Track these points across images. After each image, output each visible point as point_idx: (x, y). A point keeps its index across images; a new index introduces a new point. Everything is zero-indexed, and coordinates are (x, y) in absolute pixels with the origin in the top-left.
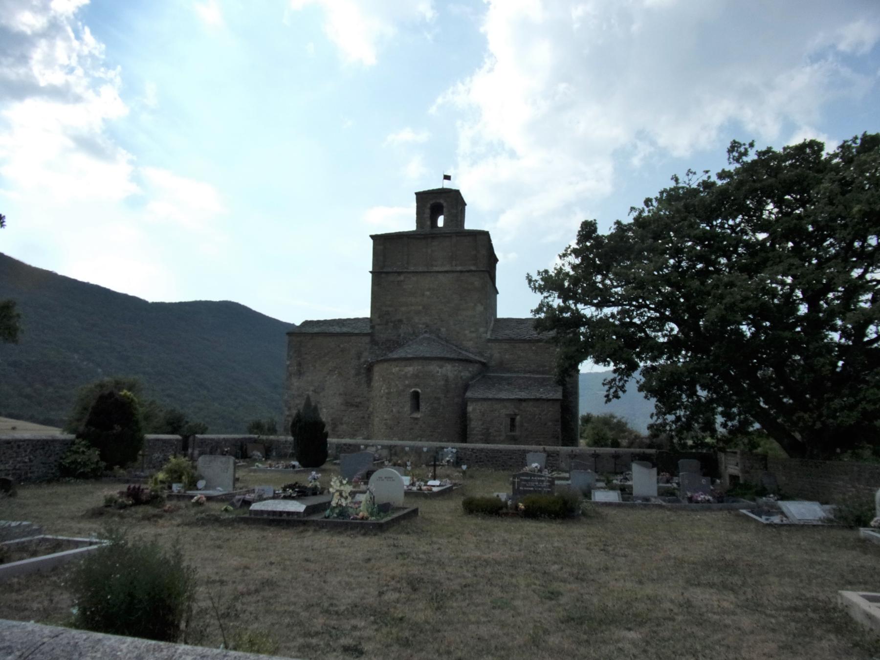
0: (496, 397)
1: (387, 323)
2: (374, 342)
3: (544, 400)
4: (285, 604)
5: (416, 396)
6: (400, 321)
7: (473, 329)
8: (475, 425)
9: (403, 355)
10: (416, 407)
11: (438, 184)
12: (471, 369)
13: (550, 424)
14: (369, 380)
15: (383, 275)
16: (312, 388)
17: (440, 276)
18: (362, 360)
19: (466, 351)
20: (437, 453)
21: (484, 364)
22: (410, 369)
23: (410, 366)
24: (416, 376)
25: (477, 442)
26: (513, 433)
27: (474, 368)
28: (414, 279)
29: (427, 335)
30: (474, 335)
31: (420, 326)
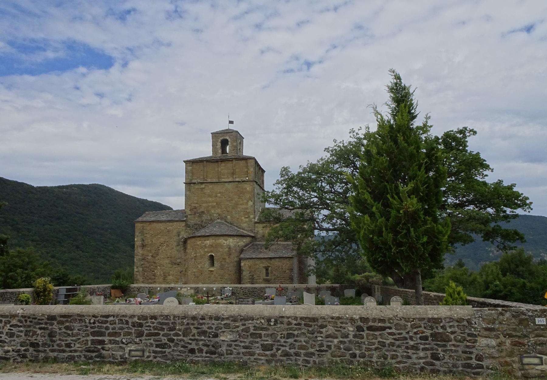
0: (257, 257)
1: (195, 214)
2: (187, 226)
3: (284, 257)
4: (143, 240)
5: (212, 257)
6: (203, 212)
7: (246, 216)
8: (246, 274)
9: (203, 234)
10: (212, 264)
11: (225, 126)
12: (244, 240)
13: (287, 271)
14: (185, 248)
15: (192, 185)
16: (151, 254)
17: (226, 184)
18: (181, 237)
19: (243, 229)
20: (221, 290)
21: (252, 237)
22: (208, 242)
23: (208, 240)
24: (211, 246)
25: (247, 283)
26: (268, 278)
27: (246, 240)
28: (211, 186)
29: (219, 221)
30: (247, 220)
31: (215, 215)
